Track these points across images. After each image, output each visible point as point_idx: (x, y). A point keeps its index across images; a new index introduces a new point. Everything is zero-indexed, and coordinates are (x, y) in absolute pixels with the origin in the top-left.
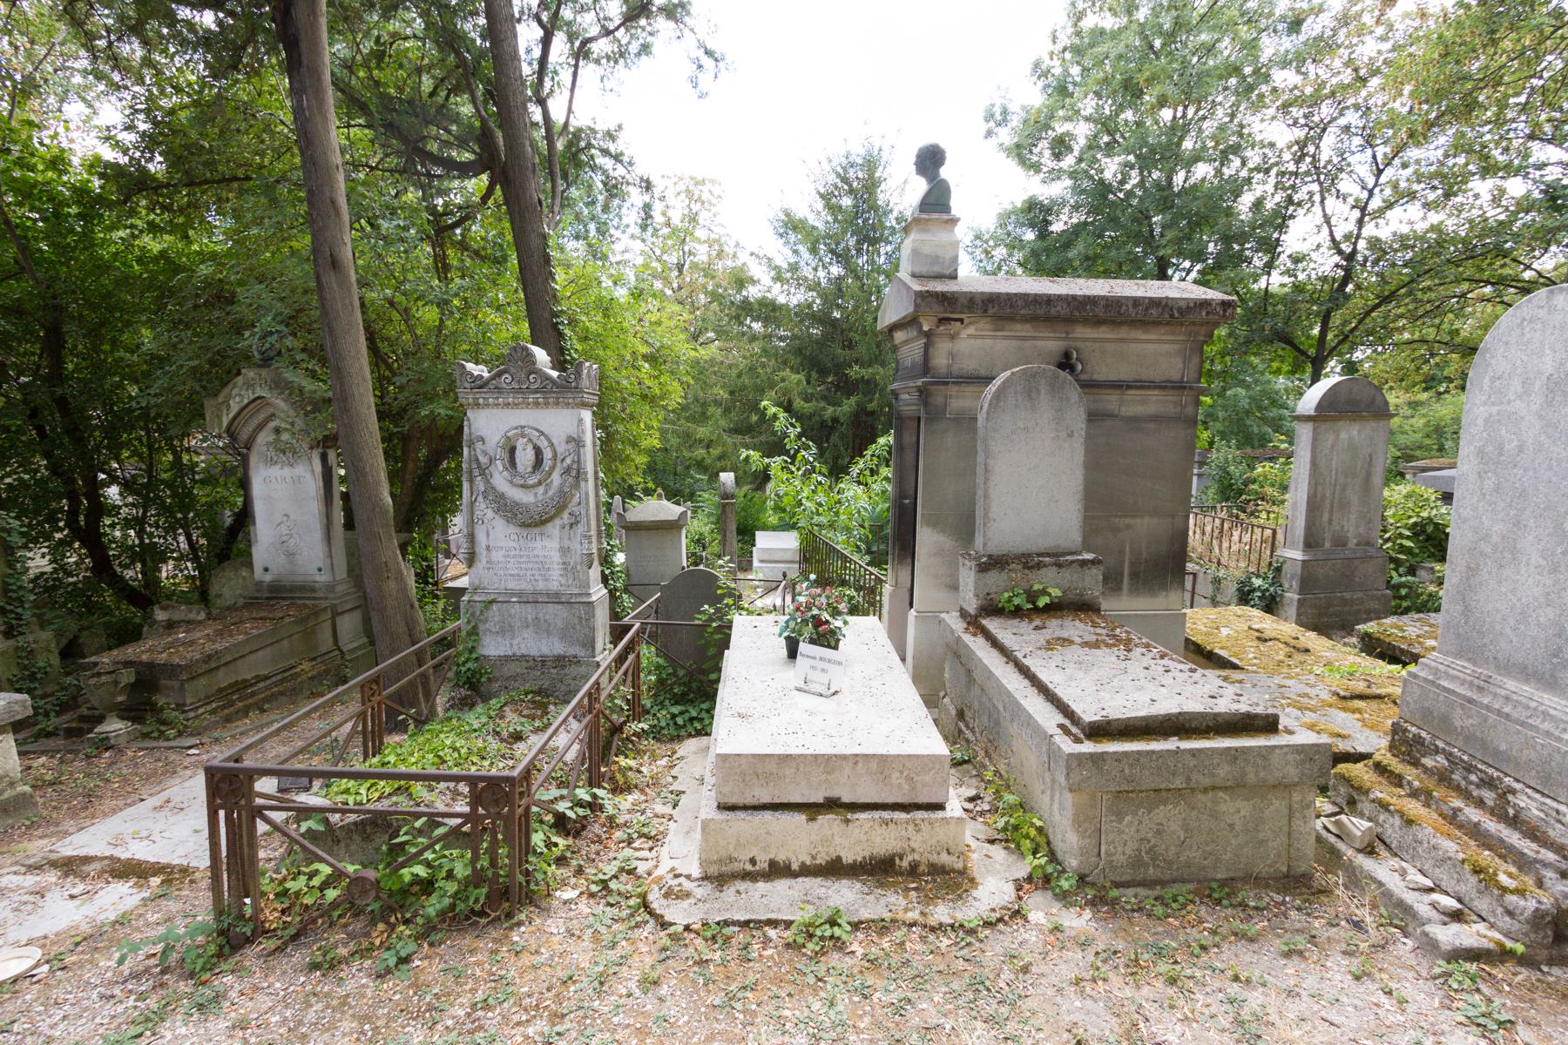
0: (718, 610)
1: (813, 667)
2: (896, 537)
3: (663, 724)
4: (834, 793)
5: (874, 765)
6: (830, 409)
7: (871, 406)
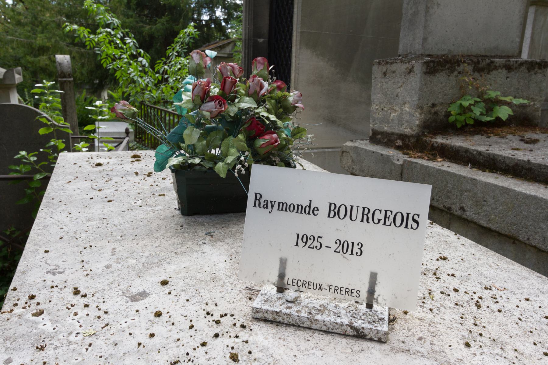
1: (305, 240)
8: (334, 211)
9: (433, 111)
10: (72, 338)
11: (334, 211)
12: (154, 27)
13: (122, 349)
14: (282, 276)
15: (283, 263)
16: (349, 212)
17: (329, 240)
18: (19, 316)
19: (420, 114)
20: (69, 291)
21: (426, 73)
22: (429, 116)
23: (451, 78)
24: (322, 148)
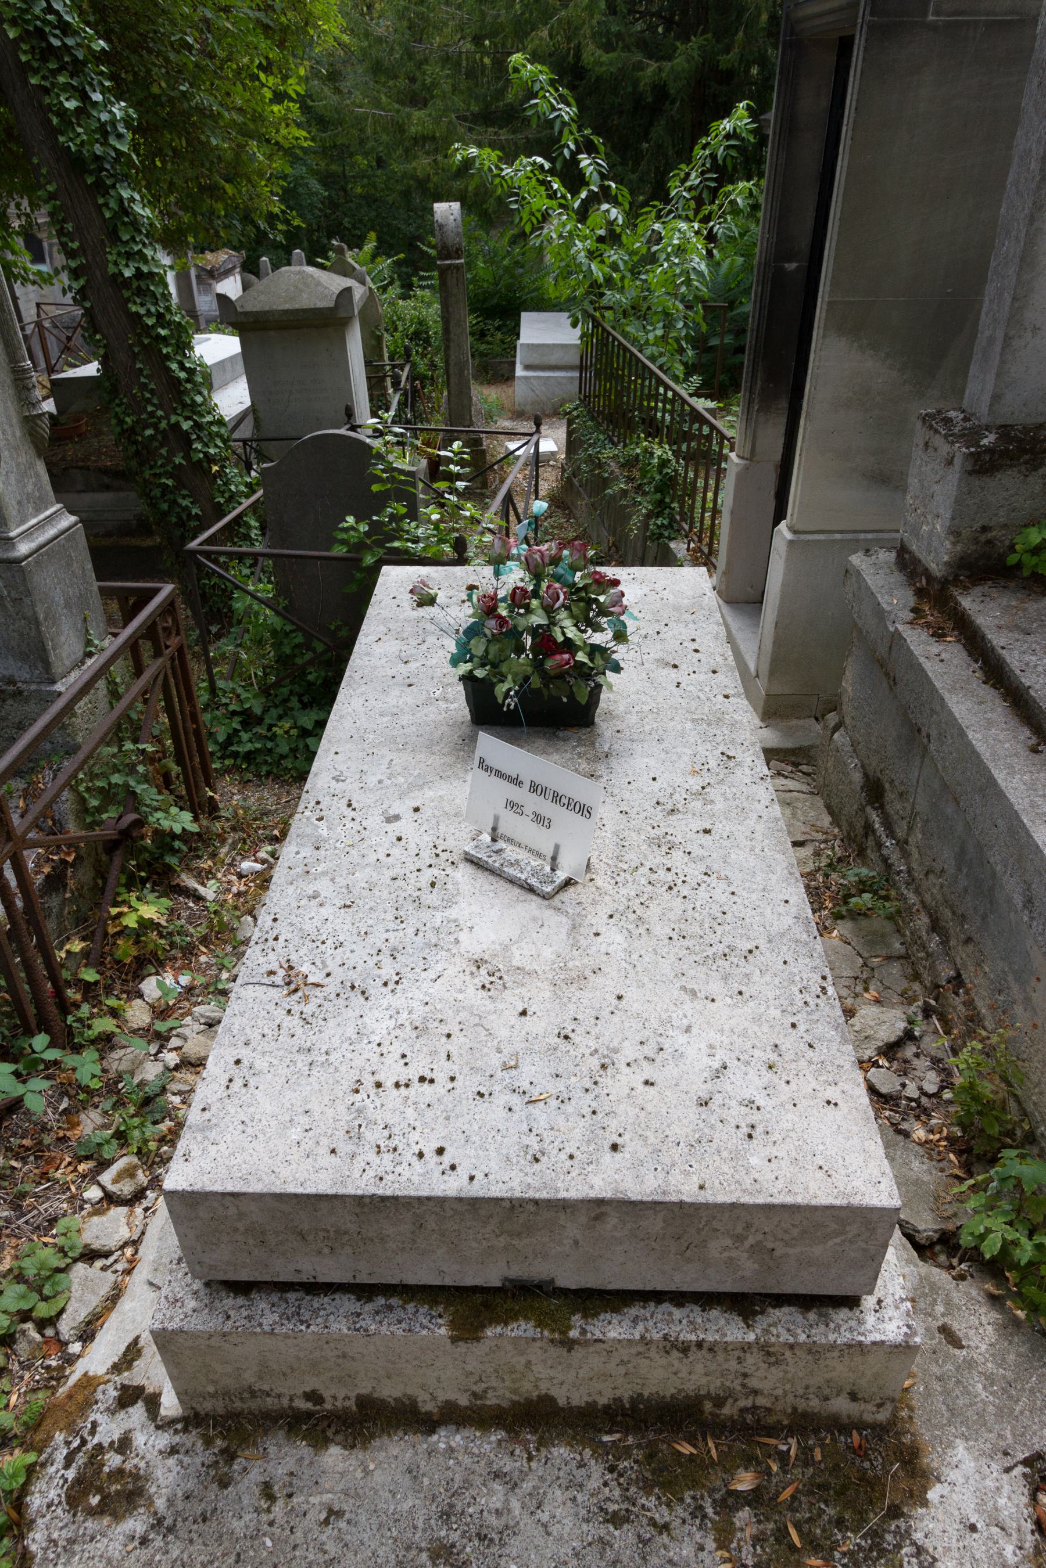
0: (375, 527)
1: (511, 805)
2: (760, 346)
3: (284, 749)
4: (537, 1270)
5: (655, 1224)
6: (652, 66)
7: (728, 60)
8: (534, 788)
9: (983, 538)
10: (338, 845)
11: (534, 788)
12: (667, 65)
13: (366, 861)
14: (494, 829)
15: (496, 819)
16: (544, 792)
17: (528, 810)
18: (308, 819)
19: (954, 544)
20: (345, 801)
21: (970, 473)
22: (974, 547)
23: (1030, 479)
24: (855, 532)
